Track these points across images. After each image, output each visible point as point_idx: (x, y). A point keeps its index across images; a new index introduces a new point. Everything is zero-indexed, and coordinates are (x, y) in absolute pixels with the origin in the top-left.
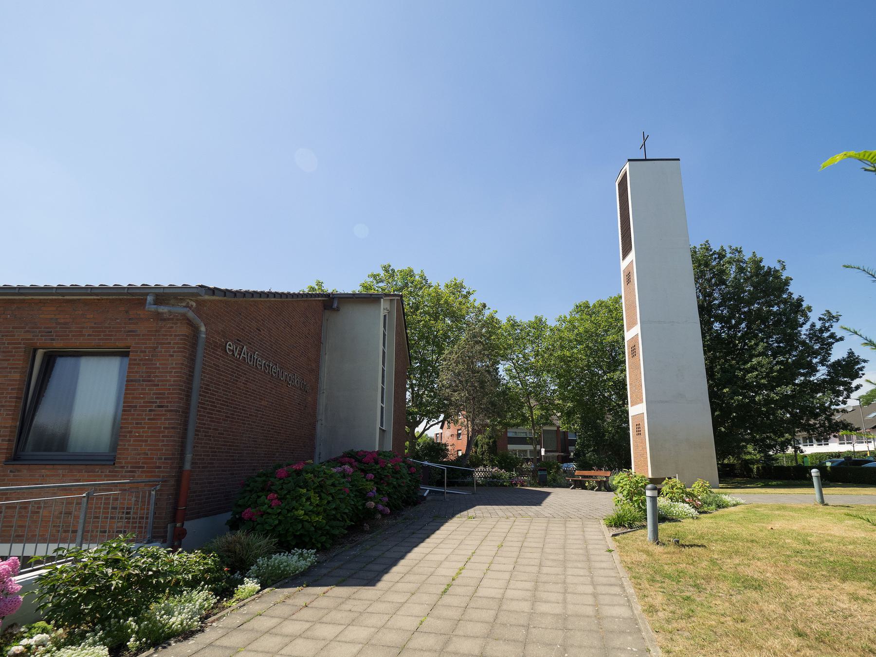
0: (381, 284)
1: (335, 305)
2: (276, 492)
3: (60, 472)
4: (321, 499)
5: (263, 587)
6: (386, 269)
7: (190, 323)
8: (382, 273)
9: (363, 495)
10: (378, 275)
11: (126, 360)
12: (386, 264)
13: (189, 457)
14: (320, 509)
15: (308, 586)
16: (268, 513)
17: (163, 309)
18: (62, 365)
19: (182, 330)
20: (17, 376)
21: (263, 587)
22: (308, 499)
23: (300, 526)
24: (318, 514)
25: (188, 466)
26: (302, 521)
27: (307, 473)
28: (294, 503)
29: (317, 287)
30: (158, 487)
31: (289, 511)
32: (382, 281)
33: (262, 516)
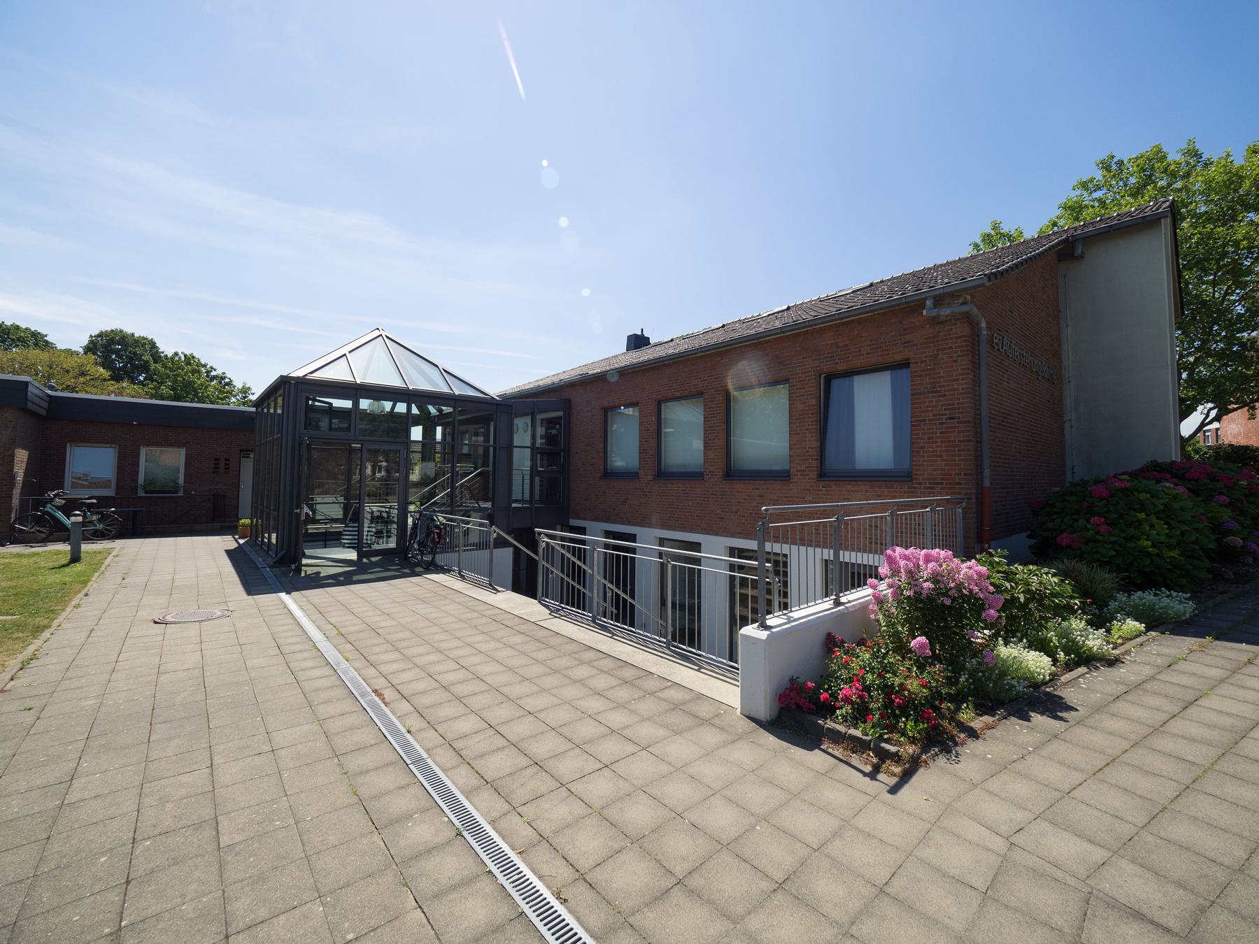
0: (1098, 194)
1: (1079, 251)
2: (1101, 515)
3: (863, 488)
4: (1171, 528)
5: (1148, 629)
6: (1106, 166)
7: (967, 317)
8: (1099, 175)
9: (1219, 529)
10: (1091, 180)
11: (904, 374)
12: (1104, 156)
13: (987, 472)
14: (1173, 541)
15: (1217, 639)
16: (1096, 541)
17: (945, 312)
18: (836, 384)
19: (963, 330)
20: (813, 402)
21: (1148, 629)
22: (1152, 526)
23: (1148, 561)
24: (1170, 548)
25: (987, 483)
26: (1149, 555)
27: (1139, 492)
28: (1132, 531)
29: (993, 233)
30: (964, 505)
31: (1127, 539)
32: (1098, 188)
33: (1086, 543)
